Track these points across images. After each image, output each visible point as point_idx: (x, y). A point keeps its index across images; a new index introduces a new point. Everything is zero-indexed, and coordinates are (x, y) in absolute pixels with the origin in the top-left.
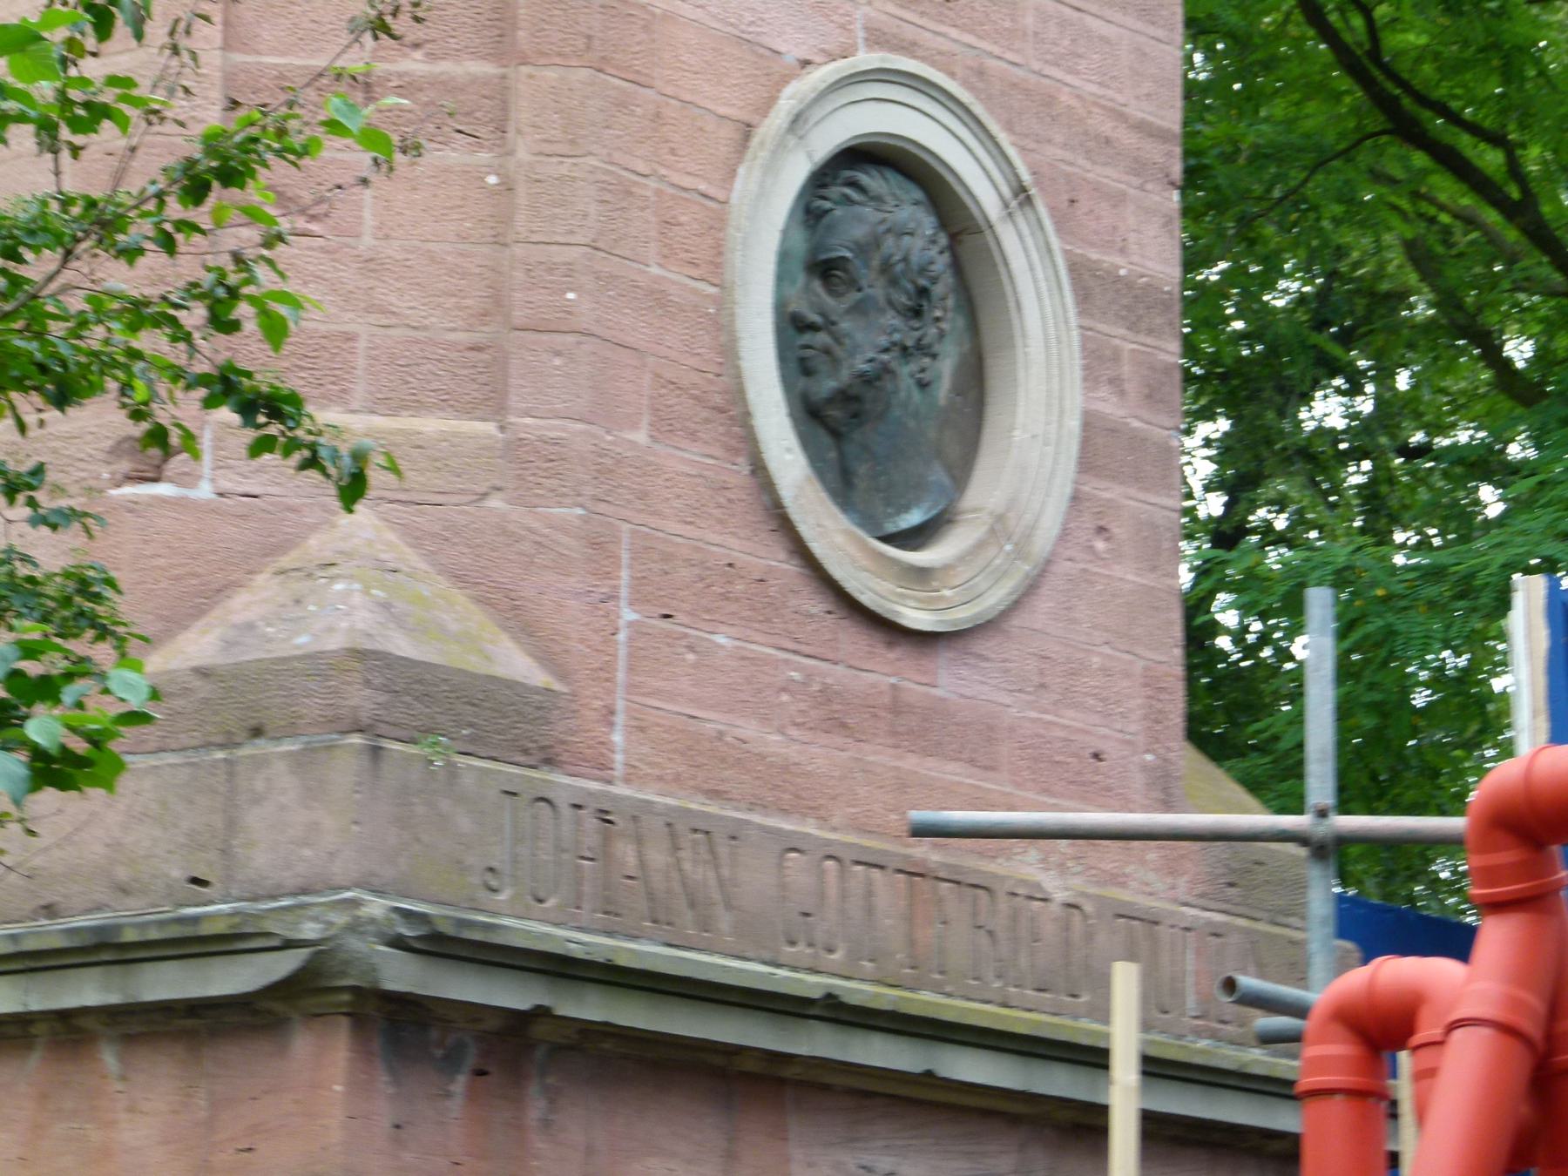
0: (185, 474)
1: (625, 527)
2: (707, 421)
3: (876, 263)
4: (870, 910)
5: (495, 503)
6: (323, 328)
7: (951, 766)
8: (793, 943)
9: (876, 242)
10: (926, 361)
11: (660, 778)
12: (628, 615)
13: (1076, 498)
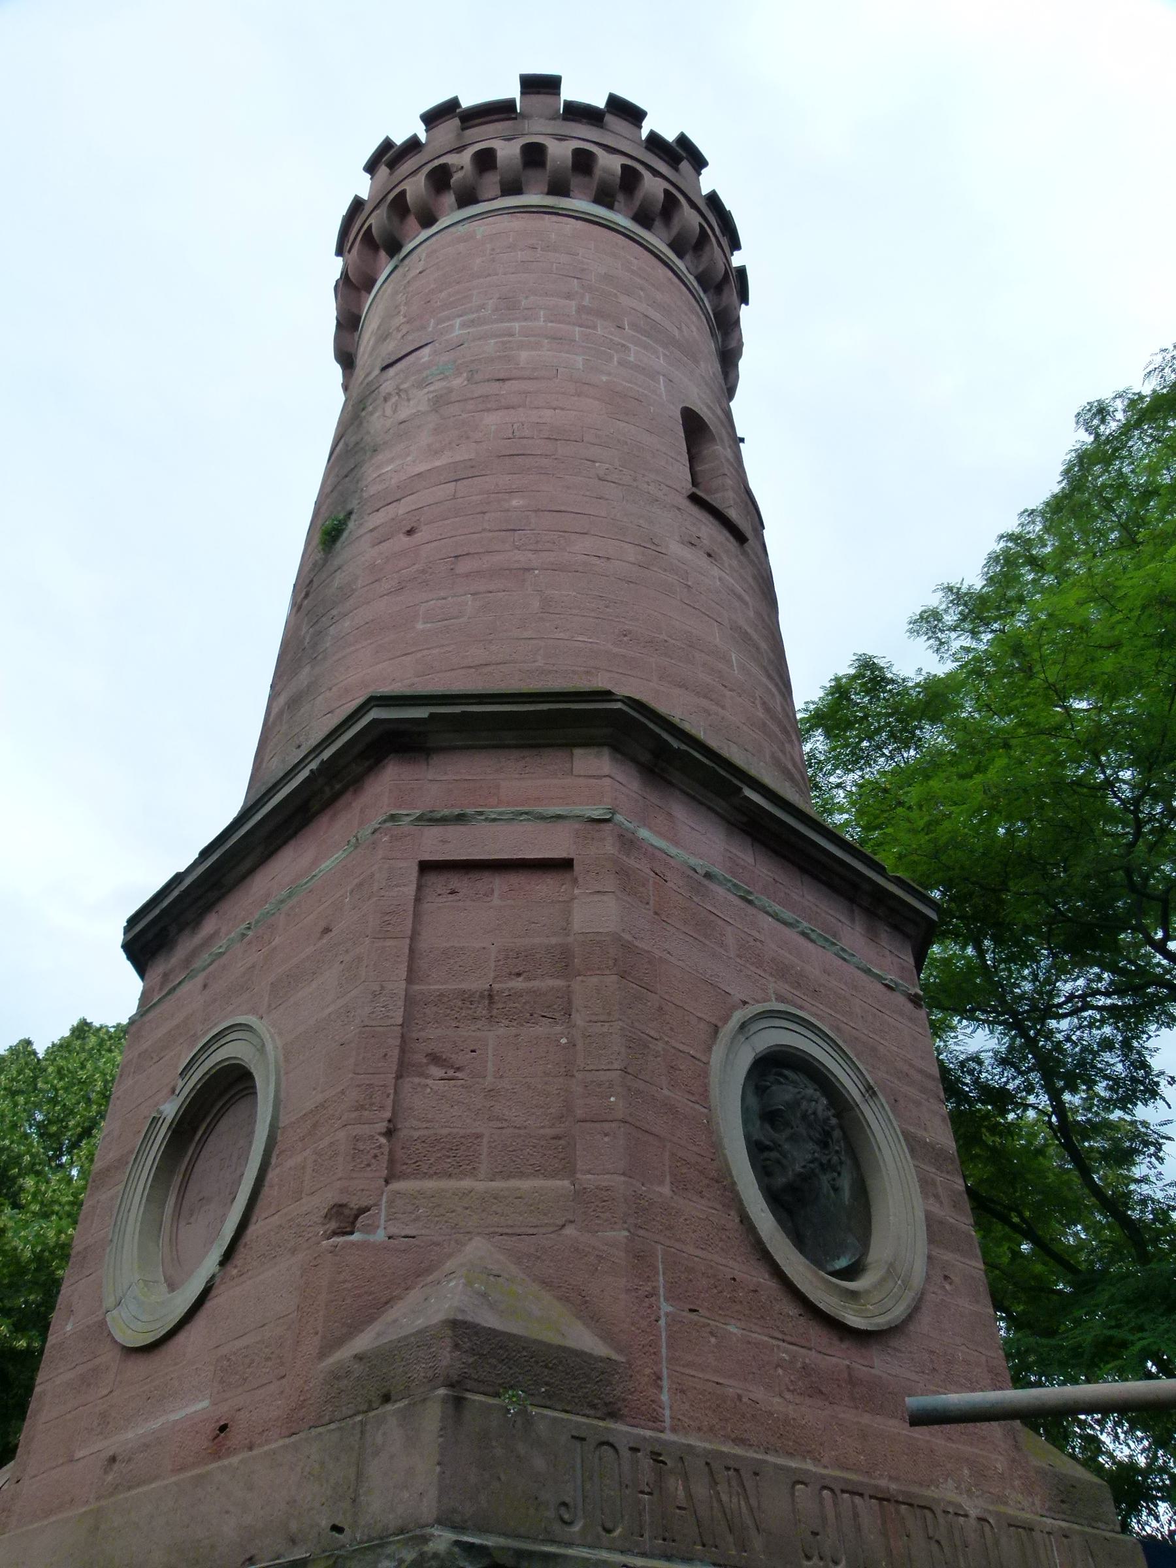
0: (369, 1225)
1: (659, 1247)
2: (708, 1186)
3: (799, 1115)
4: (859, 1529)
5: (569, 1231)
6: (462, 1132)
7: (892, 1422)
8: (808, 1558)
9: (797, 1103)
10: (835, 1174)
11: (699, 1429)
12: (666, 1308)
13: (929, 1257)
